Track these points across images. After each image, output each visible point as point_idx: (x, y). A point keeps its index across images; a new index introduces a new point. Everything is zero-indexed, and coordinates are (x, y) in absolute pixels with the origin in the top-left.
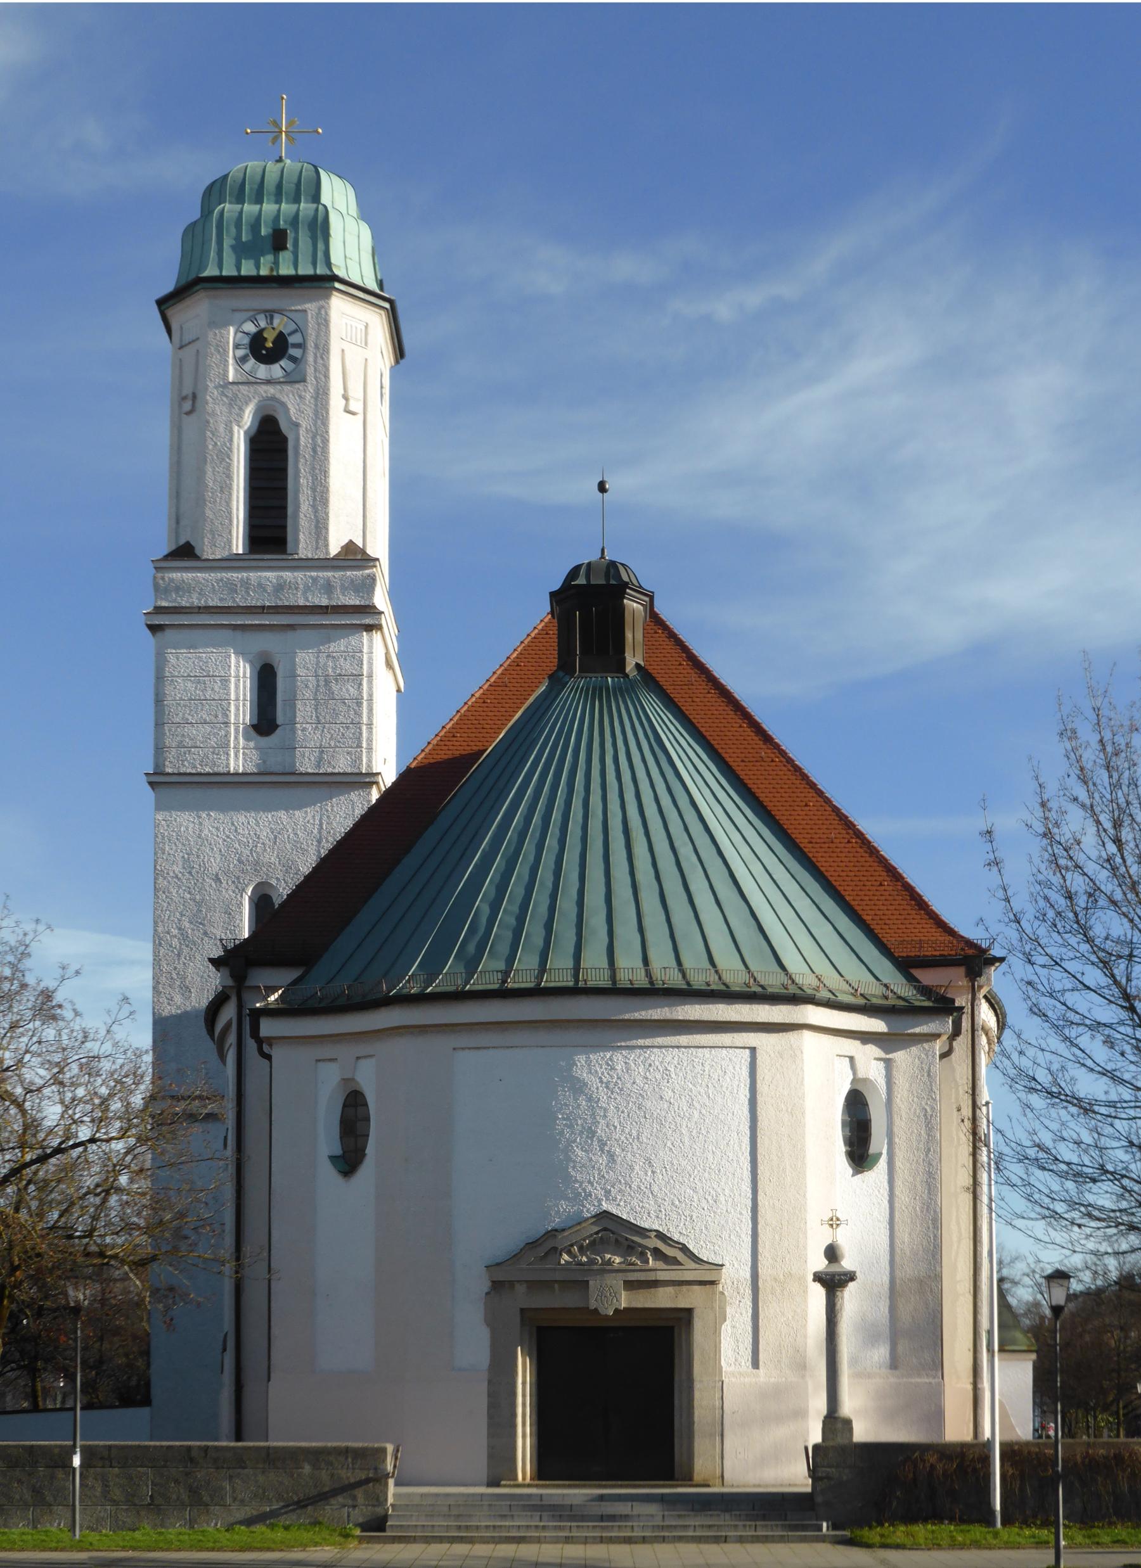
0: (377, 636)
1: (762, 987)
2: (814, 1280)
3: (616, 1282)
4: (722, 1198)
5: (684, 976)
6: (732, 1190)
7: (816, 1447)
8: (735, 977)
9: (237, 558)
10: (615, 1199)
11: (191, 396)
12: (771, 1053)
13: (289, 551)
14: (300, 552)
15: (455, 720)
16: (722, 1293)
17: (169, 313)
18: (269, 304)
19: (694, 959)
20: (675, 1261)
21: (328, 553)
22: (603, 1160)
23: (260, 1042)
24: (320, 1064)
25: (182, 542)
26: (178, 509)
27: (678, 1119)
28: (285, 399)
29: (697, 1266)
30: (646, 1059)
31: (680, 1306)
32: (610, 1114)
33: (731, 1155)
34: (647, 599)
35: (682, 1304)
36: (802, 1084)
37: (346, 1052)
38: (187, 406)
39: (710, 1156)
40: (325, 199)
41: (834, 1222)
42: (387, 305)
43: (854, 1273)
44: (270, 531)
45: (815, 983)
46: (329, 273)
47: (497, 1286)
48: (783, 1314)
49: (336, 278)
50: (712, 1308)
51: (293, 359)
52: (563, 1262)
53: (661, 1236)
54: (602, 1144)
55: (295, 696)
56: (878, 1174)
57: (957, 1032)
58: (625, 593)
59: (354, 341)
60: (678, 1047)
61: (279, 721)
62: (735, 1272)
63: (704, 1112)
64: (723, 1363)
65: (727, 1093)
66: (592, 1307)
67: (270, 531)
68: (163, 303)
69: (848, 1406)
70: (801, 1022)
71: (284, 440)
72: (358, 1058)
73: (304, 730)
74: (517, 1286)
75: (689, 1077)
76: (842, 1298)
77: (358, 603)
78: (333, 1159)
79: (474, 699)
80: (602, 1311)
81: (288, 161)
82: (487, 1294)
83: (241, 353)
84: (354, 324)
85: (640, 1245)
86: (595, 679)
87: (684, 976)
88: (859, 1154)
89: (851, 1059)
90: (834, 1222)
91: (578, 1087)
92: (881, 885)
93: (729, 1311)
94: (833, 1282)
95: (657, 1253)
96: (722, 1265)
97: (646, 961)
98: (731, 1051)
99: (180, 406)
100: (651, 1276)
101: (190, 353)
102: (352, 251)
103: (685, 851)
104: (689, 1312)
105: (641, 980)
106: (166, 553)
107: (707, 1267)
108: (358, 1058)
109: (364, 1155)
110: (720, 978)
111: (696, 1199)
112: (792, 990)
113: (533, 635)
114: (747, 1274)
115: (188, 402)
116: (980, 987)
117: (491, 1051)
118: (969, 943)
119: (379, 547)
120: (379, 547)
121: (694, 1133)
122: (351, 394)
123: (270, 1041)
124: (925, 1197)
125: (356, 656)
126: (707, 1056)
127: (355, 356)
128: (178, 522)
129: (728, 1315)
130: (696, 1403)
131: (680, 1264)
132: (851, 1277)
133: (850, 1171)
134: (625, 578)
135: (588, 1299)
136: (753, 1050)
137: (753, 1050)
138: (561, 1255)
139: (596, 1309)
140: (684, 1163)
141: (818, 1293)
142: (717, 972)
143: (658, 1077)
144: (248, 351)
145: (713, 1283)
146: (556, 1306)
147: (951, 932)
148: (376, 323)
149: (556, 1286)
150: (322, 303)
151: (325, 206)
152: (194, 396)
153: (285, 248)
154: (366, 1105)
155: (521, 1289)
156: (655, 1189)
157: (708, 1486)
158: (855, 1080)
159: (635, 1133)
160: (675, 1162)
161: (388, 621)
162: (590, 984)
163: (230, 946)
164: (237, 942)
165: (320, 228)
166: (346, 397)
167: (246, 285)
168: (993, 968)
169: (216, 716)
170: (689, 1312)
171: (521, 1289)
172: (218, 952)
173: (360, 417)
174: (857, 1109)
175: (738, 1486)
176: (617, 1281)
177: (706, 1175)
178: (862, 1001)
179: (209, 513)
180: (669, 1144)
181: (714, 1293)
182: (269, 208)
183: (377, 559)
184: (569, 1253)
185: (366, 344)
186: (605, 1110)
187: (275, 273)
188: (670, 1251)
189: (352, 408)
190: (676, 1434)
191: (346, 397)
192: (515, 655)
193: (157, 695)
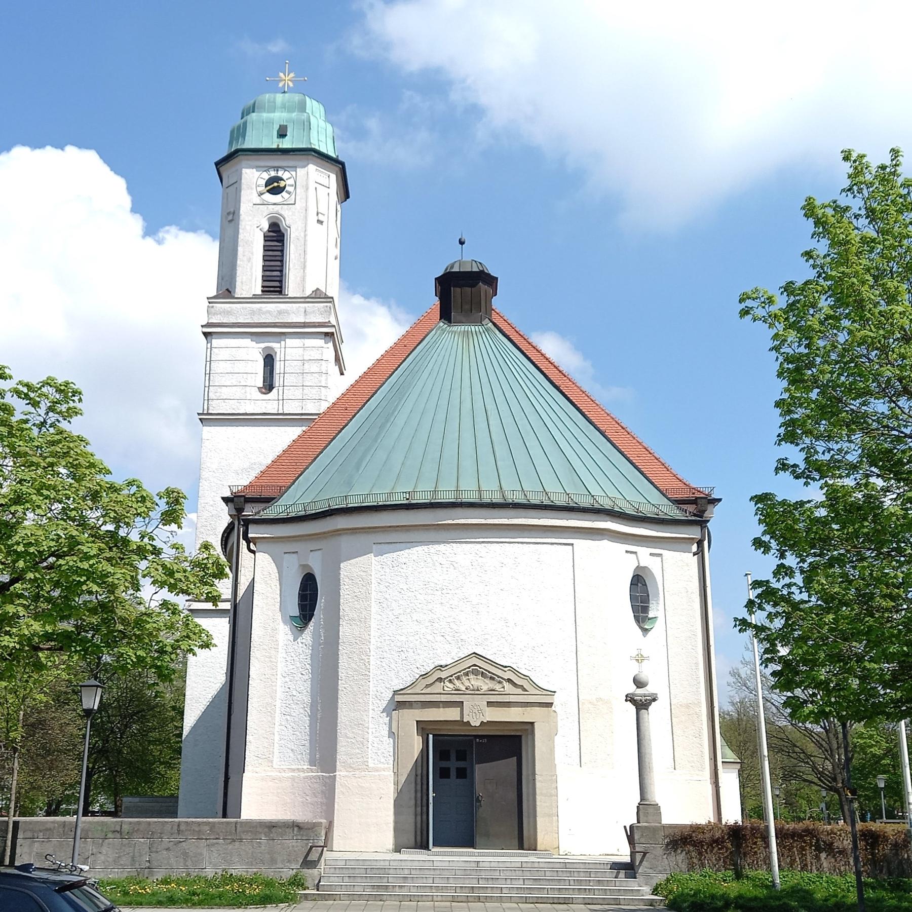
18: (276, 164)
23: (248, 541)
28: (282, 212)
38: (230, 217)
44: (274, 284)
67: (274, 284)
68: (217, 164)
69: (658, 795)
101: (232, 190)
112: (596, 506)
123: (255, 540)
145: (550, 705)
152: (234, 213)
165: (306, 126)
172: (228, 494)
179: (308, 667)
188: (516, 680)
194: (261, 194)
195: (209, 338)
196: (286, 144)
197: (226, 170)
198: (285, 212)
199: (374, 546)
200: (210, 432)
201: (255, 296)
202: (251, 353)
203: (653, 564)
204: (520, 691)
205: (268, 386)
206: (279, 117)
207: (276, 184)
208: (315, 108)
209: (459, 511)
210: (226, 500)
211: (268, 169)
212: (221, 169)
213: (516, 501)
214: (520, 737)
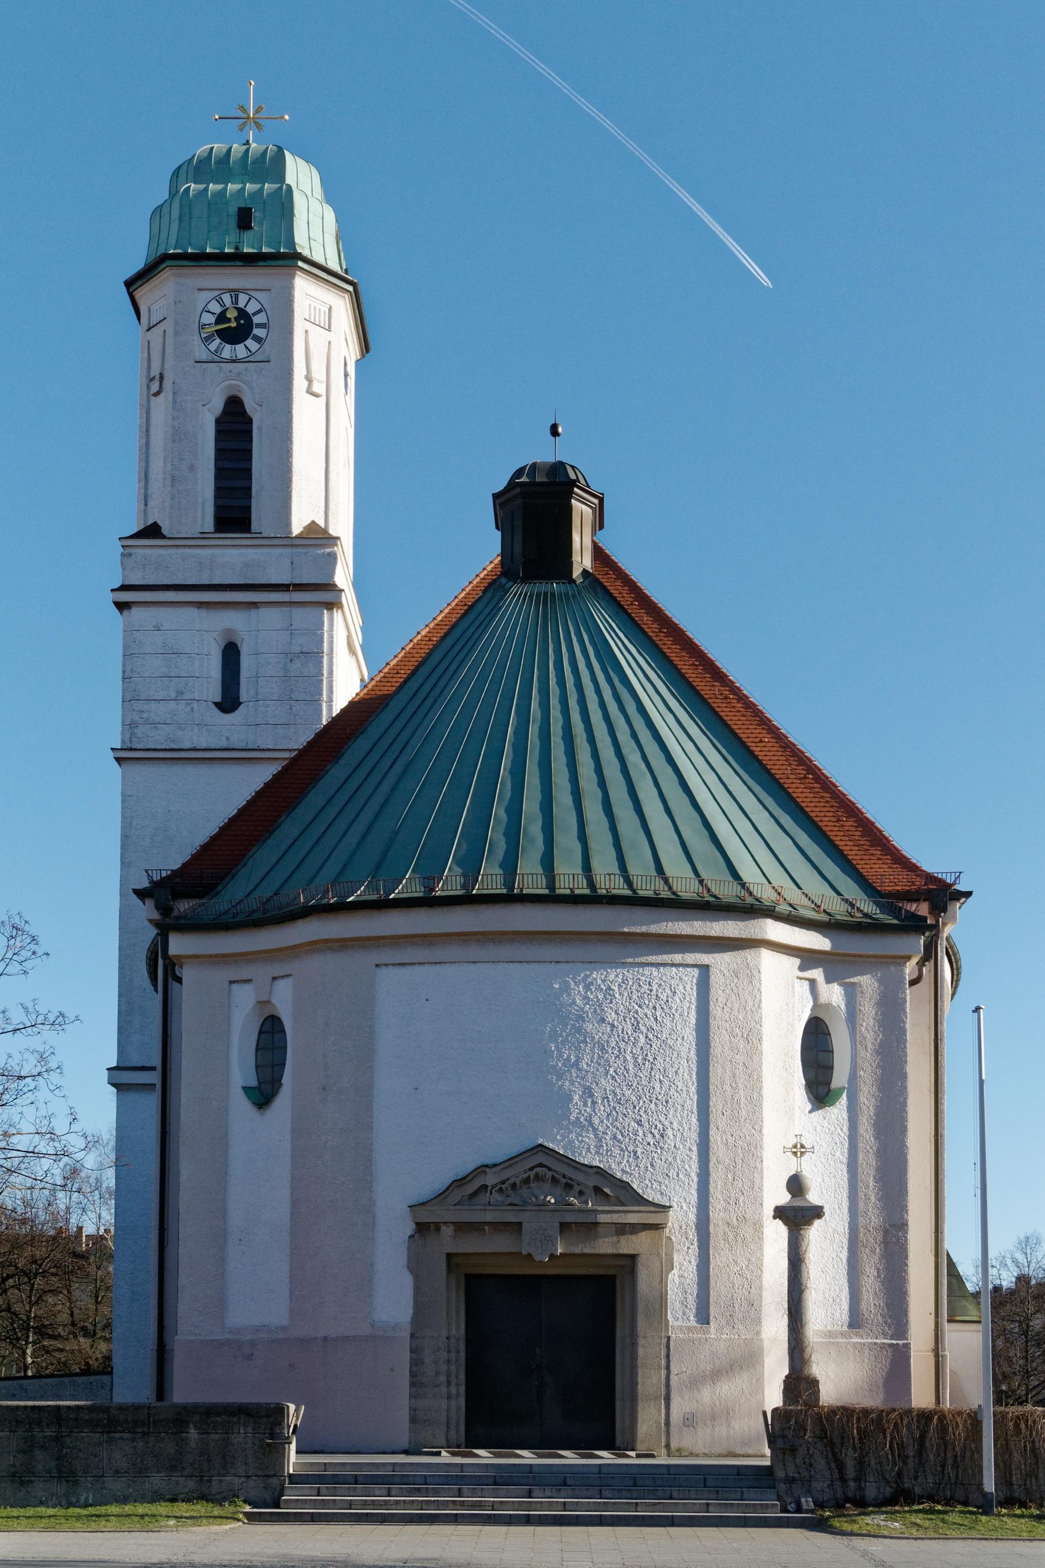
0: (337, 615)
1: (715, 896)
4: (670, 1132)
6: (680, 1124)
7: (775, 1411)
8: (687, 888)
11: (158, 376)
12: (726, 971)
19: (640, 867)
24: (234, 986)
25: (150, 522)
26: (146, 489)
27: (622, 1045)
30: (587, 977)
31: (621, 1252)
33: (680, 1084)
34: (596, 501)
35: (625, 1250)
36: (759, 1007)
37: (261, 972)
38: (155, 387)
39: (657, 1085)
40: (290, 179)
42: (351, 288)
43: (822, 1208)
45: (774, 896)
47: (423, 1229)
48: (736, 1263)
50: (658, 1255)
51: (258, 340)
56: (838, 1111)
57: (930, 953)
58: (572, 492)
59: (320, 327)
61: (243, 696)
62: (681, 1217)
63: (650, 1036)
64: (670, 1317)
65: (676, 1015)
66: (525, 1252)
67: (234, 514)
68: (129, 284)
70: (759, 937)
72: (274, 979)
74: (443, 1228)
75: (634, 997)
78: (246, 1089)
79: (419, 637)
81: (254, 145)
84: (318, 307)
86: (540, 587)
88: (820, 1090)
97: (587, 867)
99: (148, 387)
102: (316, 233)
103: (633, 758)
104: (633, 1257)
106: (135, 531)
108: (274, 979)
109: (281, 1085)
111: (641, 1133)
113: (482, 576)
117: (417, 968)
118: (930, 878)
119: (342, 526)
120: (342, 526)
121: (640, 1060)
122: (314, 375)
125: (315, 634)
126: (655, 974)
129: (676, 1264)
132: (817, 1212)
133: (809, 1106)
134: (573, 476)
139: (529, 1255)
140: (628, 1093)
141: (776, 1234)
143: (601, 997)
146: (487, 1251)
148: (341, 307)
151: (289, 187)
152: (162, 377)
155: (447, 1231)
156: (596, 1121)
157: (652, 1456)
158: (816, 1006)
160: (618, 1091)
161: (349, 598)
163: (156, 877)
164: (164, 874)
165: (283, 205)
166: (309, 379)
168: (958, 905)
171: (447, 1231)
172: (145, 884)
173: (323, 399)
174: (816, 1038)
175: (692, 1454)
177: (653, 1106)
178: (824, 918)
181: (660, 1238)
183: (338, 538)
191: (309, 379)
192: (463, 595)
194: (208, 339)
201: (203, 535)
205: (229, 703)
212: (138, 295)
214: (613, 1278)
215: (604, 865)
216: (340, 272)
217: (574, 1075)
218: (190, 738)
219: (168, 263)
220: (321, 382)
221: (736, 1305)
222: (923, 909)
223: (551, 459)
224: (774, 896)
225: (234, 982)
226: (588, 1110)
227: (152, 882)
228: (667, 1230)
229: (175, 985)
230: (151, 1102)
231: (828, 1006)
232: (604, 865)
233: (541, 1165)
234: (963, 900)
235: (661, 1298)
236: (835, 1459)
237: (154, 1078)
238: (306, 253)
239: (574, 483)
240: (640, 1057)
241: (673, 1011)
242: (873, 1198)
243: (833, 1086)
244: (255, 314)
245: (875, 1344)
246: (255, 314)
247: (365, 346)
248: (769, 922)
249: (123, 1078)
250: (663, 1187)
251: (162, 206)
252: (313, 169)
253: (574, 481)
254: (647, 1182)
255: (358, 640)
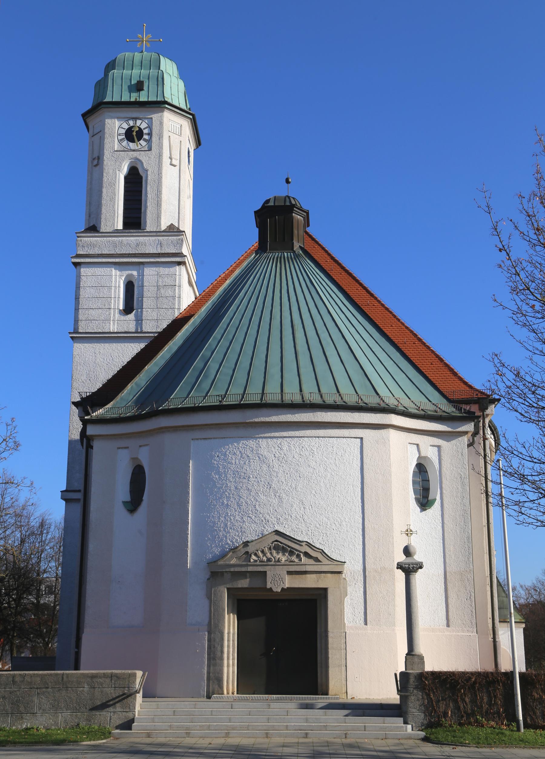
2: (397, 568)
3: (282, 571)
4: (344, 523)
5: (321, 396)
6: (350, 519)
7: (402, 673)
8: (351, 399)
9: (117, 231)
10: (282, 524)
13: (142, 228)
14: (147, 228)
15: (210, 288)
16: (345, 579)
17: (88, 120)
18: (135, 115)
20: (317, 560)
21: (160, 229)
22: (275, 501)
24: (120, 450)
25: (91, 225)
27: (319, 478)
28: (141, 158)
29: (330, 563)
32: (279, 475)
34: (305, 214)
35: (321, 585)
38: (95, 162)
41: (409, 533)
42: (191, 117)
44: (134, 219)
46: (163, 100)
49: (166, 103)
52: (252, 560)
53: (309, 545)
54: (275, 492)
55: (143, 295)
59: (174, 134)
60: (318, 437)
62: (352, 568)
65: (347, 463)
67: (134, 219)
69: (421, 648)
71: (141, 178)
72: (140, 446)
73: (147, 311)
74: (225, 574)
76: (415, 579)
77: (174, 252)
78: (125, 503)
79: (220, 278)
80: (275, 590)
82: (208, 579)
83: (120, 137)
85: (297, 550)
87: (321, 396)
88: (424, 501)
89: (418, 445)
90: (409, 533)
91: (262, 459)
92: (431, 364)
93: (349, 589)
94: (409, 570)
95: (306, 554)
96: (345, 562)
98: (348, 439)
99: (92, 163)
100: (303, 569)
101: (98, 136)
102: (175, 91)
103: (324, 336)
104: (325, 590)
105: (297, 399)
107: (336, 563)
110: (342, 399)
112: (383, 405)
114: (360, 568)
115: (97, 161)
116: (487, 415)
117: (212, 441)
121: (328, 486)
124: (462, 524)
126: (335, 442)
127: (175, 139)
128: (90, 216)
130: (330, 646)
131: (320, 562)
133: (418, 509)
134: (293, 202)
135: (266, 582)
136: (362, 439)
137: (362, 439)
138: (251, 556)
139: (271, 589)
141: (400, 575)
142: (340, 395)
143: (307, 454)
144: (124, 137)
145: (340, 573)
147: (470, 387)
148: (186, 125)
149: (248, 575)
150: (160, 114)
152: (99, 158)
153: (143, 90)
154: (144, 473)
156: (306, 517)
158: (420, 458)
159: (294, 486)
162: (268, 402)
163: (84, 396)
164: (88, 394)
165: (160, 81)
166: (171, 158)
167: (124, 106)
168: (494, 405)
169: (105, 305)
170: (325, 590)
172: (78, 399)
173: (178, 167)
176: (282, 571)
177: (335, 510)
180: (313, 492)
182: (136, 72)
183: (184, 231)
184: (256, 555)
185: (181, 134)
186: (277, 473)
187: (138, 100)
188: (314, 554)
189: (174, 162)
190: (319, 665)
191: (171, 158)
193: (76, 295)
195: (78, 267)
196: (143, 98)
197: (92, 121)
198: (143, 157)
199: (192, 442)
200: (79, 348)
202: (117, 280)
203: (431, 453)
204: (311, 562)
205: (128, 309)
206: (136, 74)
207: (134, 134)
208: (168, 67)
209: (265, 411)
210: (75, 404)
211: (127, 119)
213: (314, 402)
214: (315, 600)
215: (309, 388)
216: (186, 109)
217: (294, 494)
218: (113, 327)
219: (103, 106)
220: (177, 160)
221: (381, 615)
222: (474, 408)
223: (284, 194)
224: (396, 403)
225: (119, 448)
226: (301, 512)
227: (82, 398)
228: (344, 574)
229: (89, 449)
230: (78, 508)
231: (425, 458)
232: (309, 388)
233: (277, 541)
234: (496, 403)
235: (341, 611)
236: (438, 698)
237: (80, 496)
238: (169, 101)
239: (293, 206)
240: (328, 485)
241: (345, 461)
242: (453, 557)
243: (430, 498)
244: (144, 129)
245: (458, 635)
246: (144, 129)
247: (198, 142)
248: (393, 415)
249: (67, 496)
250: (341, 552)
251: (100, 80)
252: (173, 63)
253: (294, 205)
254: (333, 549)
255: (194, 278)
